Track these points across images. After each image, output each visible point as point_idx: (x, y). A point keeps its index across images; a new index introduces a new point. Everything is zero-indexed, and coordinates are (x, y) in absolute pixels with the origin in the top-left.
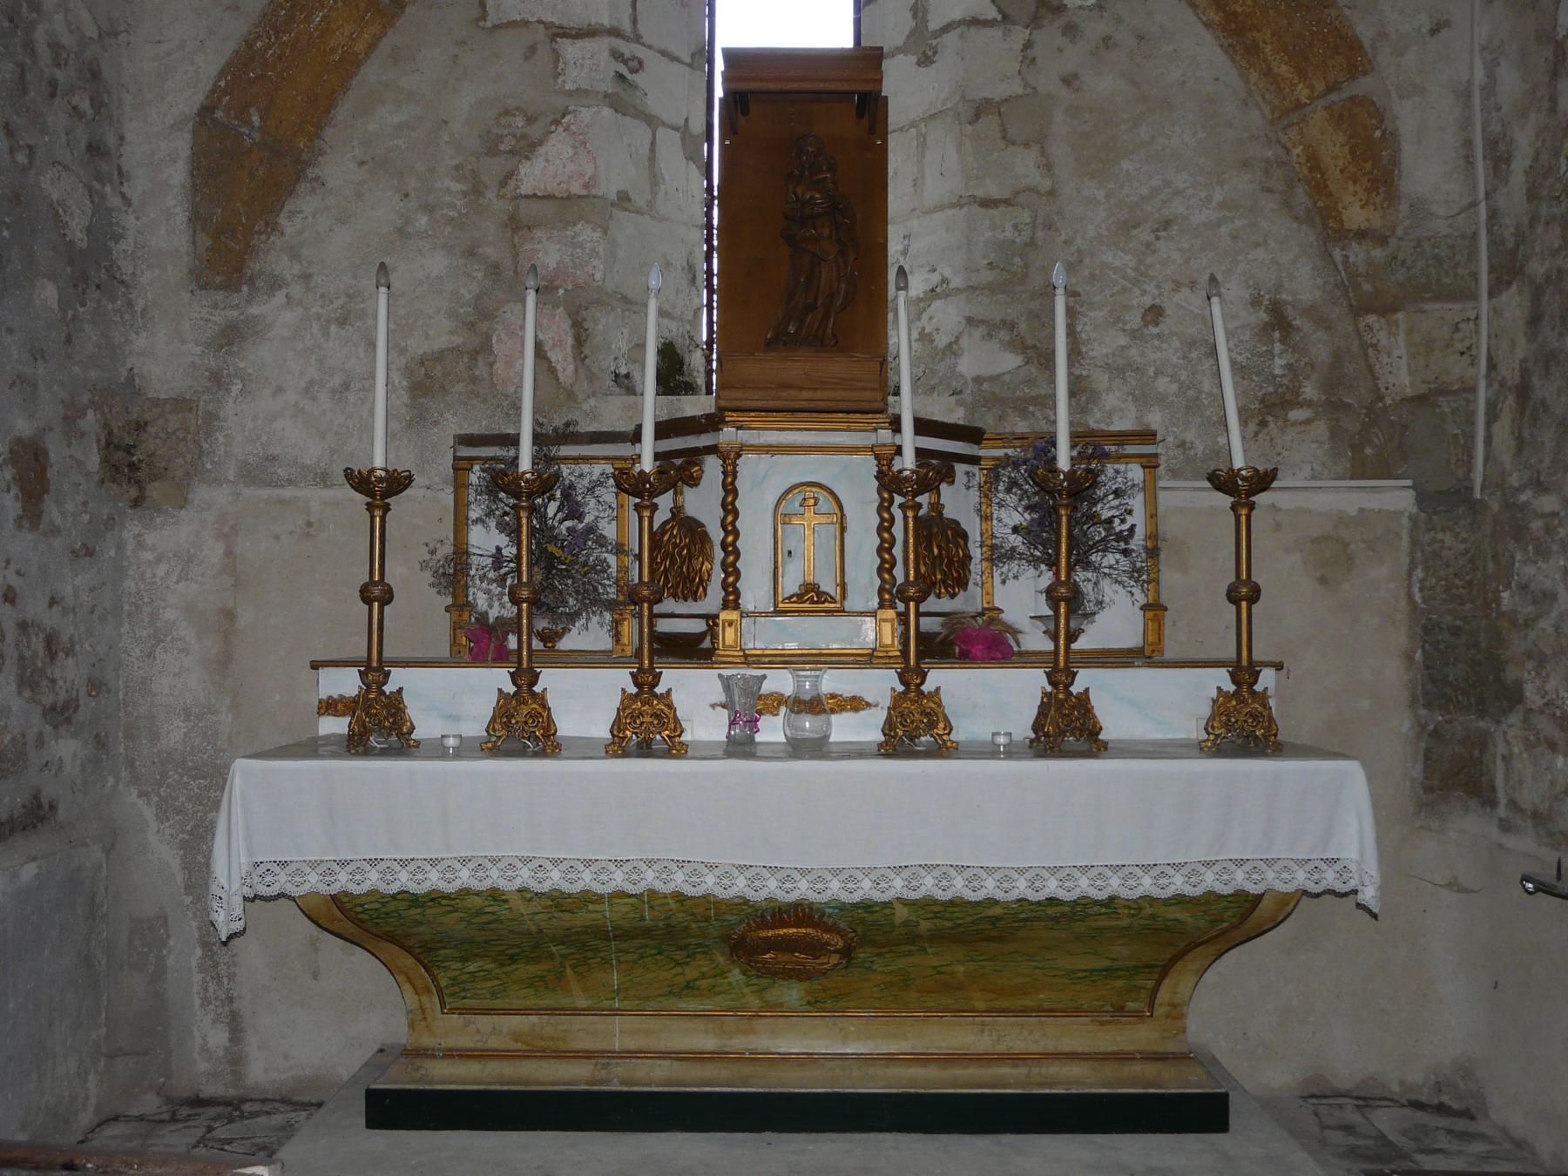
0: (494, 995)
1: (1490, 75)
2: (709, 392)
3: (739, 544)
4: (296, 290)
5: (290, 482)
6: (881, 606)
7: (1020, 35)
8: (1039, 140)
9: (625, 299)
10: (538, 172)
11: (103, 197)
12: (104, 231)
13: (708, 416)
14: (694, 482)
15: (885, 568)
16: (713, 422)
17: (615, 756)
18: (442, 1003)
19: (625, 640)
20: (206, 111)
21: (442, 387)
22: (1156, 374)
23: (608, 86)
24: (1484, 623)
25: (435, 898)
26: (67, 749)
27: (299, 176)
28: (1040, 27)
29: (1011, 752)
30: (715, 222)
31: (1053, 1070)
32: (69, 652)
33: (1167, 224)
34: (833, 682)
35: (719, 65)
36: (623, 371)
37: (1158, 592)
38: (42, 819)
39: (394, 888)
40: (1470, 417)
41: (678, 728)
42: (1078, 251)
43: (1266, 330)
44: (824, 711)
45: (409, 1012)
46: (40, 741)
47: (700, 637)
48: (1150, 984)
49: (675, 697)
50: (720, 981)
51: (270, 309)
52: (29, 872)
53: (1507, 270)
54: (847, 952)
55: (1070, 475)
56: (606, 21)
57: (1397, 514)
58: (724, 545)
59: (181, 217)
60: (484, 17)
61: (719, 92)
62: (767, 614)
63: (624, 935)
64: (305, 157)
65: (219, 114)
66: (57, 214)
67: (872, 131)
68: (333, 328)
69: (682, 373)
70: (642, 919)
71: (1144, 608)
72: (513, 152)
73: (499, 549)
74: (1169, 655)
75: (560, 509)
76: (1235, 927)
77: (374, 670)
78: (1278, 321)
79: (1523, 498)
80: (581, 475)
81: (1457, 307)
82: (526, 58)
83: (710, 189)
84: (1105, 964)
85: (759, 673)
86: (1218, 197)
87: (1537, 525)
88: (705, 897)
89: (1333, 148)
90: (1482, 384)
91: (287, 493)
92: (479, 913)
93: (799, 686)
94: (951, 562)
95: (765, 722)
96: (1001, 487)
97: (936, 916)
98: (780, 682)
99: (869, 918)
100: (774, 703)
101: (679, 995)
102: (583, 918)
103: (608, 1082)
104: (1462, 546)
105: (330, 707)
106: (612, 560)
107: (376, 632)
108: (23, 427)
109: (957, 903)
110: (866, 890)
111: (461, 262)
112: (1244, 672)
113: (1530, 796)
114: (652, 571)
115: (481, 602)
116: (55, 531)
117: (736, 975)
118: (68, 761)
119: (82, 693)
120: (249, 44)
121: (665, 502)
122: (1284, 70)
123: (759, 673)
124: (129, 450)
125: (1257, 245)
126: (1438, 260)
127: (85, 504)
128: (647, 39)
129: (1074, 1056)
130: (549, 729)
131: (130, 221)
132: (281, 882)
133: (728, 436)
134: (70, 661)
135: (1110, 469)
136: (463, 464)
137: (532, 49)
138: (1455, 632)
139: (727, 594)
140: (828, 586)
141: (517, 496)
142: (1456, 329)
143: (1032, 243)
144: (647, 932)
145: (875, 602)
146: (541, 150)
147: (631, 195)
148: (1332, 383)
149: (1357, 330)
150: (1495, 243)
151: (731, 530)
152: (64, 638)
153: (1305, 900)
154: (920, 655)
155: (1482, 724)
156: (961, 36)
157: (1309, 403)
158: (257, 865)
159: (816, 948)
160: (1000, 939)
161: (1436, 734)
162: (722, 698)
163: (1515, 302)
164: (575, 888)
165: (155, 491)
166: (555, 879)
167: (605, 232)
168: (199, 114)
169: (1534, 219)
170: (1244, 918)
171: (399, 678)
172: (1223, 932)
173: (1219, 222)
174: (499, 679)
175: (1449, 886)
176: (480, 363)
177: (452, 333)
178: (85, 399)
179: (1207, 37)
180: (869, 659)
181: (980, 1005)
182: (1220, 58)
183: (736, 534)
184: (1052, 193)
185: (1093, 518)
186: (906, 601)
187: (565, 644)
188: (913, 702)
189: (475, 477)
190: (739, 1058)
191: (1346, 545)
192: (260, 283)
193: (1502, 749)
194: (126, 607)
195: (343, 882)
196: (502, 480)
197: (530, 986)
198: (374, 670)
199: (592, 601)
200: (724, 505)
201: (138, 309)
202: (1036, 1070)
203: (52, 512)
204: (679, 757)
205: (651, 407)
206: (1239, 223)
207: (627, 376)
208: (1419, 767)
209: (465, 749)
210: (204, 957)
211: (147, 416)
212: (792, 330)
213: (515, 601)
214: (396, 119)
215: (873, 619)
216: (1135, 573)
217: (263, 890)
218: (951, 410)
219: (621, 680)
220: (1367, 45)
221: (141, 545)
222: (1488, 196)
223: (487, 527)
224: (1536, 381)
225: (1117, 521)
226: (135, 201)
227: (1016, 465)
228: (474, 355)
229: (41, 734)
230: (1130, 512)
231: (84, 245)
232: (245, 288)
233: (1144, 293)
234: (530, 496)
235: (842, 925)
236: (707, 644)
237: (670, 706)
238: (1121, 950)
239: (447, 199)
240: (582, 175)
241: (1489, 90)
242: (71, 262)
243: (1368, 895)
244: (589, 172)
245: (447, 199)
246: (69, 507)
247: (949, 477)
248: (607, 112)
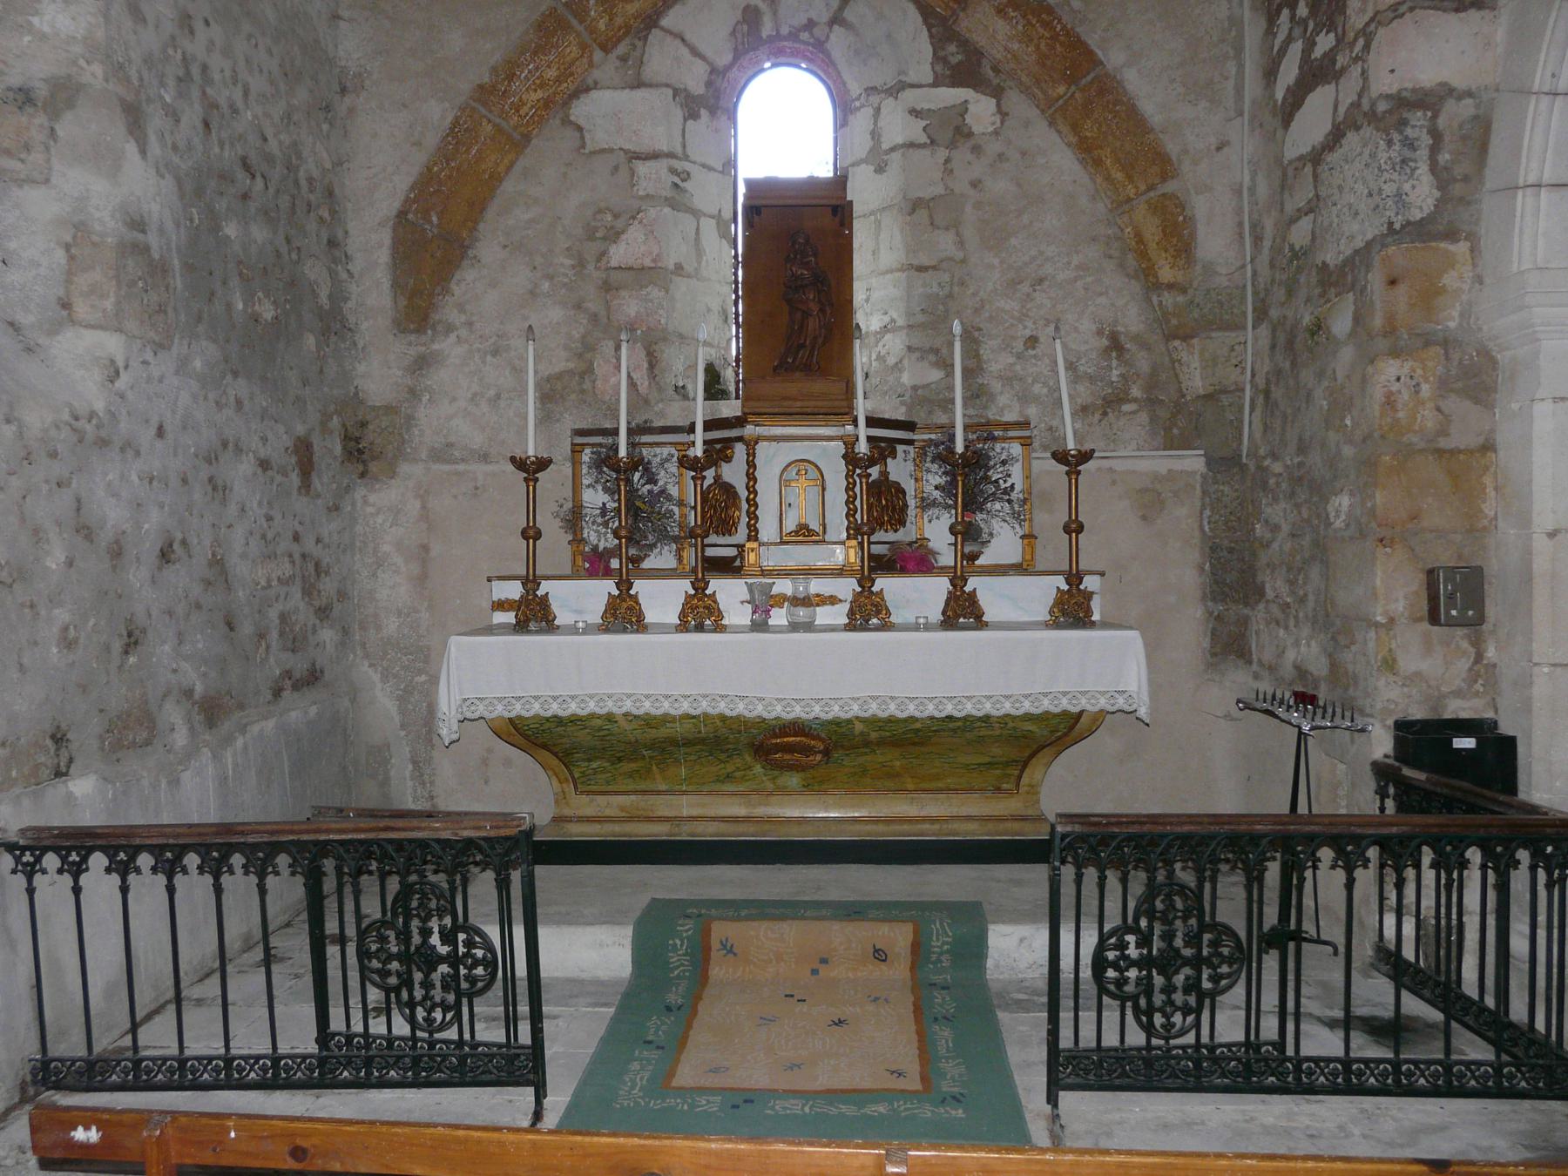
0: (608, 783)
1: (1253, 179)
2: (737, 397)
3: (757, 499)
4: (464, 332)
5: (463, 460)
6: (848, 538)
7: (942, 154)
8: (955, 226)
9: (681, 336)
10: (622, 251)
11: (337, 274)
12: (339, 296)
13: (737, 418)
14: (728, 459)
15: (850, 514)
16: (740, 422)
17: (682, 632)
18: (576, 788)
19: (685, 562)
20: (402, 214)
21: (562, 396)
22: (1033, 383)
23: (668, 192)
24: (1247, 544)
25: (575, 720)
26: (328, 635)
27: (463, 256)
28: (956, 147)
29: (928, 627)
30: (740, 279)
31: (956, 826)
32: (327, 573)
33: (1041, 281)
34: (816, 586)
35: (742, 190)
36: (681, 384)
37: (1031, 526)
38: (317, 679)
39: (549, 714)
40: (1241, 408)
41: (720, 615)
42: (982, 300)
43: (1106, 351)
44: (811, 605)
45: (555, 794)
46: (314, 632)
47: (733, 559)
48: (1016, 773)
49: (718, 596)
50: (748, 772)
51: (447, 346)
52: (313, 710)
53: (1261, 314)
54: (826, 753)
55: (962, 455)
56: (664, 147)
57: (1194, 473)
58: (748, 500)
59: (386, 284)
60: (583, 146)
61: (741, 200)
62: (776, 544)
63: (688, 743)
64: (466, 243)
65: (410, 216)
66: (314, 291)
67: (842, 224)
68: (489, 358)
69: (718, 382)
70: (700, 732)
71: (1022, 537)
72: (604, 238)
73: (604, 504)
74: (1040, 567)
75: (641, 477)
76: (1065, 735)
77: (531, 581)
78: (1115, 345)
79: (1266, 463)
80: (655, 456)
81: (1233, 335)
82: (613, 174)
83: (736, 256)
84: (987, 760)
85: (771, 581)
86: (1076, 260)
87: (1272, 481)
88: (738, 717)
89: (1152, 230)
90: (1248, 387)
91: (461, 467)
92: (600, 729)
93: (796, 589)
94: (894, 509)
95: (774, 612)
96: (928, 459)
97: (880, 728)
98: (784, 586)
99: (840, 730)
100: (780, 600)
101: (723, 782)
102: (663, 732)
103: (680, 835)
104: (1235, 494)
105: (500, 606)
106: (676, 509)
107: (531, 559)
108: (300, 429)
109: (891, 720)
110: (836, 712)
111: (572, 313)
112: (1075, 578)
113: (1267, 656)
114: (703, 517)
115: (593, 538)
116: (318, 496)
117: (758, 769)
118: (328, 641)
119: (335, 600)
120: (429, 169)
121: (710, 474)
122: (1119, 176)
123: (771, 581)
124: (358, 440)
125: (1101, 294)
126: (1221, 304)
127: (334, 477)
128: (692, 157)
129: (969, 818)
130: (640, 616)
131: (353, 288)
132: (481, 710)
133: (749, 430)
134: (328, 579)
135: (998, 447)
136: (578, 448)
137: (616, 168)
138: (1231, 550)
139: (750, 531)
140: (814, 525)
141: (618, 471)
142: (1233, 349)
143: (950, 296)
144: (702, 741)
145: (845, 535)
146: (624, 237)
147: (685, 266)
148: (1152, 384)
149: (1168, 350)
150: (1255, 293)
151: (752, 490)
152: (324, 564)
153: (1109, 716)
154: (871, 569)
155: (1246, 611)
156: (903, 155)
157: (1135, 400)
158: (465, 700)
159: (807, 750)
160: (922, 744)
161: (1219, 618)
162: (748, 597)
163: (1264, 331)
164: (659, 712)
165: (374, 467)
166: (647, 707)
167: (667, 292)
168: (398, 216)
169: (1273, 281)
170: (1072, 728)
171: (545, 587)
172: (1059, 738)
173: (1076, 279)
174: (608, 586)
175: (1225, 717)
176: (587, 380)
177: (567, 360)
178: (332, 408)
179: (1069, 153)
180: (840, 572)
181: (910, 786)
182: (1077, 167)
183: (756, 493)
184: (963, 261)
185: (986, 479)
186: (862, 535)
187: (646, 564)
188: (867, 598)
189: (586, 456)
190: (760, 821)
191: (1160, 494)
192: (439, 328)
193: (1255, 627)
194: (358, 544)
195: (518, 710)
196: (606, 460)
197: (630, 776)
198: (531, 581)
199: (664, 537)
200: (747, 474)
201: (360, 347)
202: (945, 826)
203: (316, 483)
204: (721, 632)
205: (700, 411)
206: (1089, 279)
207: (683, 387)
208: (1208, 639)
209: (589, 630)
210: (414, 769)
211: (368, 418)
212: (790, 360)
213: (616, 534)
214: (527, 216)
216: (1017, 516)
217: (469, 715)
218: (897, 409)
219: (685, 586)
220: (1174, 159)
221: (366, 502)
222: (1252, 261)
223: (596, 490)
224: (1273, 388)
225: (1001, 482)
226: (356, 276)
227: (937, 445)
228: (582, 375)
229: (314, 625)
230: (1009, 476)
231: (327, 307)
232: (429, 332)
233: (1025, 327)
234: (625, 472)
235: (823, 735)
236: (737, 563)
237: (715, 602)
238: (997, 751)
239: (562, 270)
240: (651, 253)
241: (1252, 190)
242: (321, 321)
243: (1143, 712)
244: (656, 251)
245: (562, 270)
246: (325, 480)
247: (894, 455)
248: (667, 210)
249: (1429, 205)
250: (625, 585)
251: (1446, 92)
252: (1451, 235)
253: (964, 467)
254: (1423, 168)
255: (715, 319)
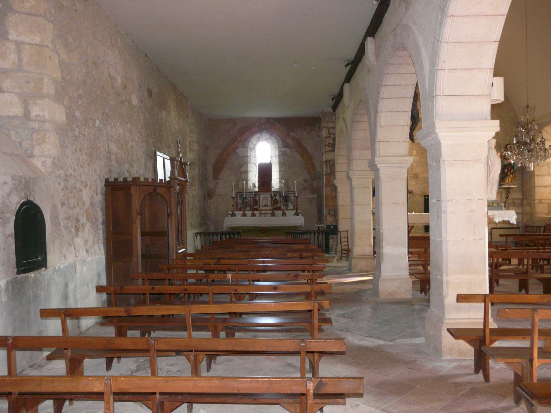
20: (214, 165)
43: (304, 182)
77: (233, 212)
78: (306, 181)
98: (263, 212)
140: (267, 205)
171: (235, 212)
198: (233, 212)
215: (260, 195)
249: (329, 172)
250: (244, 212)
251: (331, 160)
252: (331, 175)
253: (519, 147)
254: (329, 168)
255: (254, 177)
